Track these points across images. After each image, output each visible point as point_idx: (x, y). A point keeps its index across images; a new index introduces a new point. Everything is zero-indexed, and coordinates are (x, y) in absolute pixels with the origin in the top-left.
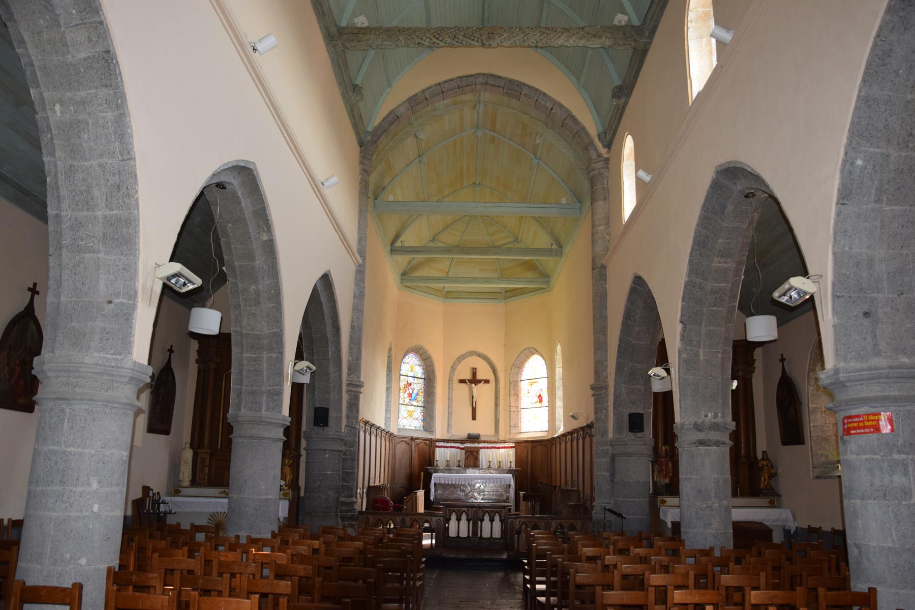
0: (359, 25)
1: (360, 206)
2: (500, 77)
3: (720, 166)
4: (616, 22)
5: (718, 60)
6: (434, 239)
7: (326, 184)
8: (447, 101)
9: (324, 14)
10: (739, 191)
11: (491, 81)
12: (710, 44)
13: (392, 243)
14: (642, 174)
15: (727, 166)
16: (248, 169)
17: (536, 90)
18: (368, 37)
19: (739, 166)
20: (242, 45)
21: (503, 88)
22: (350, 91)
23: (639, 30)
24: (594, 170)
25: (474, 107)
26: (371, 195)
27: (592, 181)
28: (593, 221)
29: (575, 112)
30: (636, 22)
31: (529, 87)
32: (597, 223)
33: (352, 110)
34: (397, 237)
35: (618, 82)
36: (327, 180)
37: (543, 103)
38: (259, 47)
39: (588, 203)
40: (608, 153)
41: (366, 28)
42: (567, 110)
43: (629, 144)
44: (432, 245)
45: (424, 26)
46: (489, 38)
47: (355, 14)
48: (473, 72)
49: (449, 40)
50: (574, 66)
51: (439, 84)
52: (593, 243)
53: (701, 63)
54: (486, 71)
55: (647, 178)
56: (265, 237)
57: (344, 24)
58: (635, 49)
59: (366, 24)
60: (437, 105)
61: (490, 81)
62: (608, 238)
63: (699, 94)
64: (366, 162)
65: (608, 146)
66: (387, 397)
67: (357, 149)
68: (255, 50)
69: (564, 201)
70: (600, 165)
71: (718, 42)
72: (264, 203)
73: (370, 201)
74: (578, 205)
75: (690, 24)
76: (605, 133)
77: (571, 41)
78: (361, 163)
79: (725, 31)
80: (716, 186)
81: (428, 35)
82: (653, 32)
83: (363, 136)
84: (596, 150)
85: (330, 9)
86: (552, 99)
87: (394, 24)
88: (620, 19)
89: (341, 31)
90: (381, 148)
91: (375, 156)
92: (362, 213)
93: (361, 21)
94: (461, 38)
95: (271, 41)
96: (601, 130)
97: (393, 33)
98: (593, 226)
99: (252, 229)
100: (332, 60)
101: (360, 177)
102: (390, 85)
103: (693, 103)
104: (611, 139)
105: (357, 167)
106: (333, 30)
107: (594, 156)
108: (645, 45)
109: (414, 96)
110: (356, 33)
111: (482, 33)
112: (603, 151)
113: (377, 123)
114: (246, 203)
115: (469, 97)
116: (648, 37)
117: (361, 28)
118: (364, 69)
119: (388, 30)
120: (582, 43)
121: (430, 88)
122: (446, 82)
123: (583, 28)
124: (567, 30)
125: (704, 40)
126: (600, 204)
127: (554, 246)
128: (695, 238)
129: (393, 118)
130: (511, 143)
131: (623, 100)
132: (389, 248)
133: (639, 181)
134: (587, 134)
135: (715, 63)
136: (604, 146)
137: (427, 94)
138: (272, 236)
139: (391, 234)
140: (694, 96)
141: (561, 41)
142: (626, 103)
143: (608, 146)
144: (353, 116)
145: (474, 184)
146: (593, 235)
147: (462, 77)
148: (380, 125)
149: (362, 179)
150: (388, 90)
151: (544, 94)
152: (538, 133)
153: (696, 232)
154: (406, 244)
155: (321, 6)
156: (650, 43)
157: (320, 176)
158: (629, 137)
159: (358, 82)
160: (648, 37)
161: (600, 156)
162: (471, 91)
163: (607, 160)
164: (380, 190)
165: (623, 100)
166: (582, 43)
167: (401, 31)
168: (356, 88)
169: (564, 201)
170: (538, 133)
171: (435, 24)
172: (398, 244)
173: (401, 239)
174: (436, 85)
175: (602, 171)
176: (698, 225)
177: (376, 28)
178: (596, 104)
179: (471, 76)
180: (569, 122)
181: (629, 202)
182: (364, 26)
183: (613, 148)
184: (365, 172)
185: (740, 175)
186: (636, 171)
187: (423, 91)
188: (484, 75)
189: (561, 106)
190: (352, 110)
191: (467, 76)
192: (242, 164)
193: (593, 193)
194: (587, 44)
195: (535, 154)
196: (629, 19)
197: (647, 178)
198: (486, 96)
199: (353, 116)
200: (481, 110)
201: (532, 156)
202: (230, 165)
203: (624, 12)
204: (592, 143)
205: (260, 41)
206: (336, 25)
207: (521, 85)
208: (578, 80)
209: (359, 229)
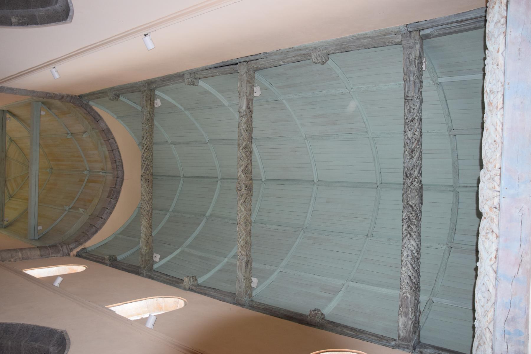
0: (155, 102)
1: (38, 92)
2: (121, 185)
3: (66, 333)
4: (155, 255)
5: (135, 321)
6: (12, 140)
7: (54, 70)
8: (107, 153)
9: (164, 81)
10: (49, 349)
11: (119, 180)
12: (145, 312)
13: (9, 112)
14: (60, 280)
15: (66, 338)
16: (67, 17)
17: (114, 208)
18: (149, 107)
19: (67, 347)
20: (149, 27)
21: (115, 187)
22: (116, 93)
23: (151, 269)
24: (62, 247)
25: (103, 169)
26: (45, 100)
27: (54, 246)
28: (25, 249)
29: (99, 233)
30: (155, 266)
31: (116, 203)
32: (24, 252)
33: (103, 93)
34: (14, 115)
35: (119, 258)
36: (57, 71)
37: (106, 212)
38: (147, 37)
39: (38, 244)
40: (74, 255)
41: (154, 105)
42: (101, 228)
43: (79, 268)
44: (7, 139)
45: (154, 141)
46: (146, 180)
47: (162, 100)
48: (124, 169)
49: (145, 155)
50: (129, 231)
51: (118, 148)
52: (9, 250)
53: (132, 310)
54: (125, 177)
55: (57, 283)
56: (14, 20)
57: (157, 92)
58: (139, 267)
59: (156, 106)
60: (105, 146)
61: (119, 180)
62: (13, 260)
63: (114, 312)
64: (68, 99)
65: (78, 255)
66: (418, 272)
67: (78, 94)
68: (146, 35)
69: (40, 228)
70: (66, 251)
71: (147, 319)
72: (41, 24)
73: (41, 99)
74: (37, 238)
75: (155, 299)
76: (87, 252)
77: (144, 229)
78: (68, 96)
79: (153, 323)
80: (52, 332)
81: (148, 143)
82: (150, 277)
83: (86, 98)
84: (75, 247)
85: (165, 85)
86: (107, 218)
87: (156, 123)
88: (157, 257)
89: (152, 91)
90: (78, 109)
91: (72, 104)
92: (32, 93)
93: (158, 103)
94: (146, 163)
95: (151, 46)
96: (89, 249)
97: (150, 121)
98: (21, 249)
99: (20, 11)
100: (136, 84)
101: (58, 93)
102: (118, 118)
103: (107, 308)
104: (84, 256)
105: (65, 93)
106: (154, 86)
107: (71, 246)
108: (142, 273)
109: (111, 132)
110: (151, 100)
111: (150, 176)
112: (75, 252)
113: (95, 108)
114: (41, 11)
115: (109, 166)
116: (147, 275)
117: (154, 103)
118: (130, 103)
119: (152, 119)
120: (143, 235)
121: (116, 142)
122: (119, 152)
123: (151, 235)
124: (150, 226)
125: (146, 309)
126: (38, 253)
127: (6, 223)
128: (12, 324)
129: (97, 119)
130: (80, 192)
131: (108, 262)
132: (5, 109)
133: (53, 279)
134: (86, 241)
135: (132, 319)
136: (78, 252)
137: (112, 140)
138: (14, 25)
139: (16, 111)
140: (112, 309)
141: (144, 223)
142: (106, 264)
143: (78, 255)
144: (99, 93)
145: (52, 169)
146: (14, 250)
147: (122, 163)
148: (93, 110)
149: (56, 95)
150: (115, 116)
151: (111, 213)
152: (86, 209)
153: (17, 324)
154: (8, 122)
155: (168, 80)
156: (143, 276)
157: (59, 67)
158: (84, 268)
159: (121, 98)
160: (147, 275)
161: (72, 250)
162: (113, 168)
163: (69, 255)
164: (49, 106)
165: (108, 262)
166: (143, 235)
167: (152, 126)
168: (117, 97)
169: (40, 228)
170: (86, 209)
171: (155, 147)
172: (8, 116)
173: (12, 118)
174: (117, 146)
175: (61, 252)
176: (22, 324)
177: (153, 112)
178: (104, 246)
179: (123, 168)
180: (93, 229)
181: (38, 273)
182: (155, 105)
183: (78, 259)
184: (62, 98)
185: (60, 348)
186: (61, 276)
187: (114, 138)
188: (123, 176)
189: (103, 224)
190: (103, 93)
191: (122, 165)
192: (70, 14)
193: (46, 247)
194: (142, 239)
195: (72, 208)
196: (157, 262)
197: (57, 283)
198: (110, 177)
199: (99, 93)
200: (101, 174)
201: (71, 207)
202: (70, 5)
203: (161, 259)
204: (80, 244)
205: (151, 39)
206: (156, 88)
207: (117, 198)
208: (119, 234)
209: (20, 90)
